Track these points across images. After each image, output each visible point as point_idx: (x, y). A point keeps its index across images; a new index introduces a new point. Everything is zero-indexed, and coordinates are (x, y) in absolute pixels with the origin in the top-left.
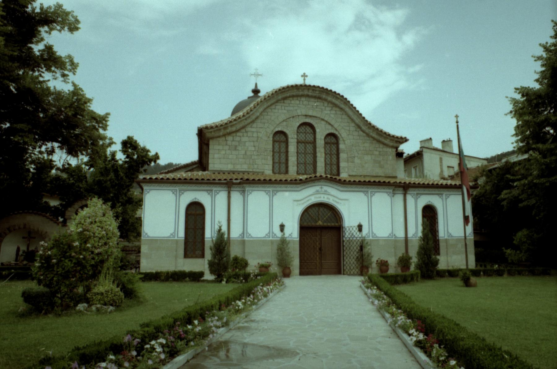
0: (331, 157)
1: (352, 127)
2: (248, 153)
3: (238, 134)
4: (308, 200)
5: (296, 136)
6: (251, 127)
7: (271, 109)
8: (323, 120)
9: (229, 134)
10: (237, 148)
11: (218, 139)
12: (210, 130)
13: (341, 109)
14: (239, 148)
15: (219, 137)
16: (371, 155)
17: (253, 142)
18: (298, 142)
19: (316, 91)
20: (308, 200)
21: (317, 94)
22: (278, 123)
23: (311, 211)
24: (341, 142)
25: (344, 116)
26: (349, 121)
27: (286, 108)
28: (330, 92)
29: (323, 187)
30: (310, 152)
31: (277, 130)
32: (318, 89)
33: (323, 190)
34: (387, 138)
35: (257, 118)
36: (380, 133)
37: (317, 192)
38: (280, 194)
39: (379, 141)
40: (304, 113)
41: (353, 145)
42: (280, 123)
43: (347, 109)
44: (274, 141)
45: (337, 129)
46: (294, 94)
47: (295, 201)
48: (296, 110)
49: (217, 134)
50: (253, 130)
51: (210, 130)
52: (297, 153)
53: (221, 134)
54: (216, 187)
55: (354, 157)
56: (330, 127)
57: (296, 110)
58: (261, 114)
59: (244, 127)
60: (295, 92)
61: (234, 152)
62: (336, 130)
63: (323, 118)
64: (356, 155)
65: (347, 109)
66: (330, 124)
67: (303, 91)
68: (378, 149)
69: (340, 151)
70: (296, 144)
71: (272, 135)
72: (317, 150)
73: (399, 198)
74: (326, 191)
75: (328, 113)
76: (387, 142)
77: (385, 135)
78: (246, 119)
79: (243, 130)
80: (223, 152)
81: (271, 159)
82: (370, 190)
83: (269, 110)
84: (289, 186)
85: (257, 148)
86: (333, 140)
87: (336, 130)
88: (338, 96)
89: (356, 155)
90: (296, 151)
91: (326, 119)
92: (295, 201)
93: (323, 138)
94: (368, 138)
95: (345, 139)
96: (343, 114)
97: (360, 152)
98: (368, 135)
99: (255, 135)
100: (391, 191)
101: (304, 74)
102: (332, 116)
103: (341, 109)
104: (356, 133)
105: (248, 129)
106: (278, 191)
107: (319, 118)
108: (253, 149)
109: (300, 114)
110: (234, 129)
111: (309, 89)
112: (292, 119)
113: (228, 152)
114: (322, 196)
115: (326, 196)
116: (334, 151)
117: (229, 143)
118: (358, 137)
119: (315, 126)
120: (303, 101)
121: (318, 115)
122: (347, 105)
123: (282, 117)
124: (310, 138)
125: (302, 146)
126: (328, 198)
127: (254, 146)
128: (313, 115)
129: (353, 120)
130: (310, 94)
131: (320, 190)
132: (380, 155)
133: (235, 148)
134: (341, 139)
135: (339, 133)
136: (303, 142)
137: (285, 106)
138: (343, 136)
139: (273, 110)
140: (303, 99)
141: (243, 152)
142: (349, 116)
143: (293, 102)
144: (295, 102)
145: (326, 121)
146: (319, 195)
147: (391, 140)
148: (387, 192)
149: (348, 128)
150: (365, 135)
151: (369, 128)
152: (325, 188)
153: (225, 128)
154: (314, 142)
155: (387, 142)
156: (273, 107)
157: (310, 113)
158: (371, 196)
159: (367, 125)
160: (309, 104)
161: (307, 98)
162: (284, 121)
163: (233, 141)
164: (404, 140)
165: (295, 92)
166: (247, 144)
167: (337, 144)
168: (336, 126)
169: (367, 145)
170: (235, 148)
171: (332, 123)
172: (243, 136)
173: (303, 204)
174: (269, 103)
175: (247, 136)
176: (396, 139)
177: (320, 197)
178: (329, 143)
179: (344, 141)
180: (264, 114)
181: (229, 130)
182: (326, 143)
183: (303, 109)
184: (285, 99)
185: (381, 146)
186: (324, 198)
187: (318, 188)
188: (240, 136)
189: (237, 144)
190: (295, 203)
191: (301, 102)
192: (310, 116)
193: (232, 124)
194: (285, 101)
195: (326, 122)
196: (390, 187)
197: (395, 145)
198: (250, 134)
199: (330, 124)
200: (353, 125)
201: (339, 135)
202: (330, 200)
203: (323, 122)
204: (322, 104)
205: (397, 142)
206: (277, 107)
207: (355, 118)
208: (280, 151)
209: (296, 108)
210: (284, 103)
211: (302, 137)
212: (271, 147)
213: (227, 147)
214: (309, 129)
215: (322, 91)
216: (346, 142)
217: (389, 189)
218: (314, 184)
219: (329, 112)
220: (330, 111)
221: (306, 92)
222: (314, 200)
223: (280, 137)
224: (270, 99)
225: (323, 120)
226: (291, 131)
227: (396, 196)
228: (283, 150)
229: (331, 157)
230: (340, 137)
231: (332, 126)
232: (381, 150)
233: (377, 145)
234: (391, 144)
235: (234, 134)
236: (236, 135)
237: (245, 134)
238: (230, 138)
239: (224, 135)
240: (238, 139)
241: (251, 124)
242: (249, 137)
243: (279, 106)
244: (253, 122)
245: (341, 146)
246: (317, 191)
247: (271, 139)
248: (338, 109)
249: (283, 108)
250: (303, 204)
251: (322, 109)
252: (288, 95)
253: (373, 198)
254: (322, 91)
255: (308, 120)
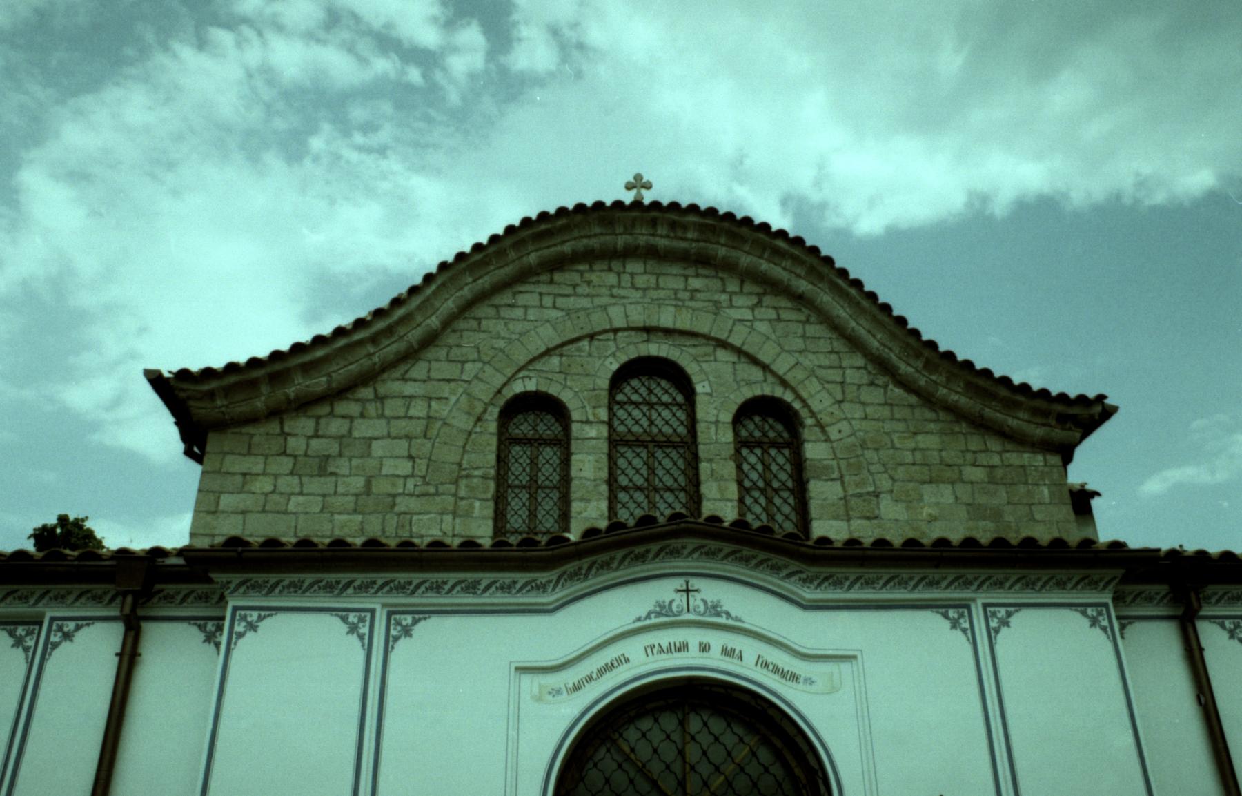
0: (770, 501)
1: (854, 369)
2: (381, 487)
3: (342, 407)
4: (609, 667)
5: (603, 414)
6: (404, 379)
7: (497, 307)
8: (723, 344)
9: (304, 404)
10: (331, 469)
11: (250, 429)
12: (206, 387)
13: (800, 299)
14: (342, 466)
15: (253, 419)
16: (953, 483)
17: (409, 437)
18: (616, 442)
19: (685, 227)
20: (609, 667)
21: (689, 241)
22: (523, 359)
23: (649, 738)
24: (808, 432)
25: (814, 329)
26: (839, 345)
27: (560, 302)
28: (744, 231)
29: (695, 583)
30: (669, 481)
31: (518, 387)
32: (692, 218)
33: (696, 601)
34: (1016, 405)
35: (430, 340)
36: (981, 382)
37: (664, 618)
38: (433, 631)
39: (981, 425)
40: (638, 316)
41: (863, 445)
42: (531, 361)
43: (825, 298)
44: (506, 441)
45: (788, 377)
46: (594, 243)
47: (523, 670)
48: (604, 308)
49: (241, 409)
50: (409, 389)
51: (206, 387)
52: (612, 481)
53: (259, 404)
54: (60, 599)
55: (877, 495)
56: (757, 374)
57: (604, 308)
58: (448, 323)
59: (368, 378)
60: (596, 238)
61: (315, 485)
62: (784, 383)
63: (723, 336)
64: (885, 483)
65: (825, 298)
66: (754, 361)
67: (628, 230)
68: (983, 459)
69: (808, 474)
70: (604, 446)
71: (494, 412)
72: (704, 467)
73: (1157, 643)
74: (715, 609)
75: (744, 317)
76: (1016, 421)
77: (1004, 392)
78: (374, 340)
79: (366, 392)
80: (264, 484)
81: (490, 512)
82: (981, 598)
83: (483, 310)
84: (486, 578)
85: (422, 465)
86: (774, 430)
87: (784, 383)
88: (781, 243)
89: (885, 483)
90: (604, 474)
91: (736, 340)
92: (523, 670)
93: (727, 417)
94: (929, 415)
95: (826, 419)
96: (807, 321)
97: (900, 473)
98: (927, 399)
99: (418, 410)
100: (1107, 598)
101: (638, 177)
102: (763, 327)
103: (800, 299)
104: (873, 396)
105: (390, 386)
106: (422, 613)
107: (707, 337)
108: (405, 467)
109: (619, 322)
110: (318, 383)
111: (654, 223)
112: (585, 343)
113: (288, 483)
114: (693, 637)
115: (717, 640)
116: (783, 476)
117: (296, 444)
118: (886, 412)
119: (691, 368)
120: (632, 275)
121: (704, 328)
122: (821, 277)
123: (547, 336)
124: (669, 421)
125: (633, 463)
126: (727, 652)
127: (411, 457)
128: (679, 325)
129: (854, 343)
130: (662, 243)
131: (680, 600)
132: (992, 481)
133: (323, 467)
134: (809, 421)
135: (798, 397)
136: (644, 445)
137: (556, 295)
138: (815, 405)
139: (505, 312)
140: (634, 266)
141: (358, 483)
142: (837, 328)
143: (594, 277)
144: (604, 278)
145: (737, 349)
146: (666, 638)
147: (1035, 412)
148: (1081, 607)
149: (835, 375)
150: (913, 399)
151: (928, 365)
152: (710, 591)
153: (278, 378)
154: (688, 445)
155: (1016, 421)
156: (505, 298)
157: (667, 318)
158: (992, 634)
159: (918, 355)
160: (658, 287)
161: (652, 265)
162: (548, 352)
163: (316, 435)
164: (1097, 409)
165: (596, 238)
166: (378, 448)
167: (795, 445)
168: (781, 367)
169: (929, 441)
170: (323, 467)
171: (766, 359)
172: (362, 416)
173: (577, 688)
174: (485, 282)
175: (381, 416)
176: (1059, 408)
177: (683, 647)
178: (759, 444)
179: (822, 427)
180: (461, 324)
181: (299, 385)
182: (741, 443)
183: (637, 302)
184: (557, 264)
185: (994, 444)
186: (704, 648)
187: (665, 591)
188: (351, 418)
189: (334, 448)
190: (530, 684)
191: (626, 278)
192: (668, 332)
193: (307, 358)
194: (558, 277)
195: (739, 351)
196: (1096, 573)
197: (1058, 434)
198: (392, 407)
199: (754, 361)
200: (859, 361)
201: (797, 405)
202: (747, 666)
203: (722, 354)
204: (715, 284)
205: (1062, 419)
206: (522, 299)
207: (860, 327)
208: (533, 479)
209: (605, 300)
210: (551, 282)
211: (634, 421)
212: (492, 458)
213: (287, 463)
214: (663, 391)
215: (712, 229)
216: (833, 432)
217: (1093, 585)
218: (639, 570)
219: (748, 315)
220: (752, 308)
221: (643, 237)
222: (642, 663)
223: (532, 417)
224: (484, 263)
225: (723, 344)
226: (582, 389)
227: (1139, 631)
228: (548, 473)
229: (770, 501)
230: (804, 413)
231: (765, 368)
232: (996, 460)
233: (975, 443)
234: (1039, 432)
235: (324, 410)
236: (332, 414)
237: (372, 409)
238: (302, 425)
239: (276, 413)
240: (336, 427)
241: (402, 368)
242: (389, 419)
243: (528, 296)
244: (410, 355)
245: (814, 451)
246: (663, 609)
247: (493, 427)
248: (784, 302)
249: (548, 301)
250: (577, 688)
251: (717, 303)
252: (567, 248)
253: (1005, 640)
254: (712, 229)
255: (656, 348)
